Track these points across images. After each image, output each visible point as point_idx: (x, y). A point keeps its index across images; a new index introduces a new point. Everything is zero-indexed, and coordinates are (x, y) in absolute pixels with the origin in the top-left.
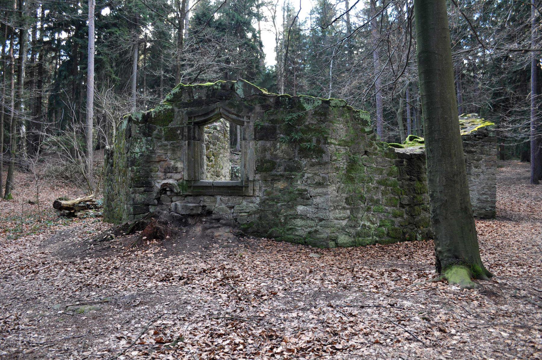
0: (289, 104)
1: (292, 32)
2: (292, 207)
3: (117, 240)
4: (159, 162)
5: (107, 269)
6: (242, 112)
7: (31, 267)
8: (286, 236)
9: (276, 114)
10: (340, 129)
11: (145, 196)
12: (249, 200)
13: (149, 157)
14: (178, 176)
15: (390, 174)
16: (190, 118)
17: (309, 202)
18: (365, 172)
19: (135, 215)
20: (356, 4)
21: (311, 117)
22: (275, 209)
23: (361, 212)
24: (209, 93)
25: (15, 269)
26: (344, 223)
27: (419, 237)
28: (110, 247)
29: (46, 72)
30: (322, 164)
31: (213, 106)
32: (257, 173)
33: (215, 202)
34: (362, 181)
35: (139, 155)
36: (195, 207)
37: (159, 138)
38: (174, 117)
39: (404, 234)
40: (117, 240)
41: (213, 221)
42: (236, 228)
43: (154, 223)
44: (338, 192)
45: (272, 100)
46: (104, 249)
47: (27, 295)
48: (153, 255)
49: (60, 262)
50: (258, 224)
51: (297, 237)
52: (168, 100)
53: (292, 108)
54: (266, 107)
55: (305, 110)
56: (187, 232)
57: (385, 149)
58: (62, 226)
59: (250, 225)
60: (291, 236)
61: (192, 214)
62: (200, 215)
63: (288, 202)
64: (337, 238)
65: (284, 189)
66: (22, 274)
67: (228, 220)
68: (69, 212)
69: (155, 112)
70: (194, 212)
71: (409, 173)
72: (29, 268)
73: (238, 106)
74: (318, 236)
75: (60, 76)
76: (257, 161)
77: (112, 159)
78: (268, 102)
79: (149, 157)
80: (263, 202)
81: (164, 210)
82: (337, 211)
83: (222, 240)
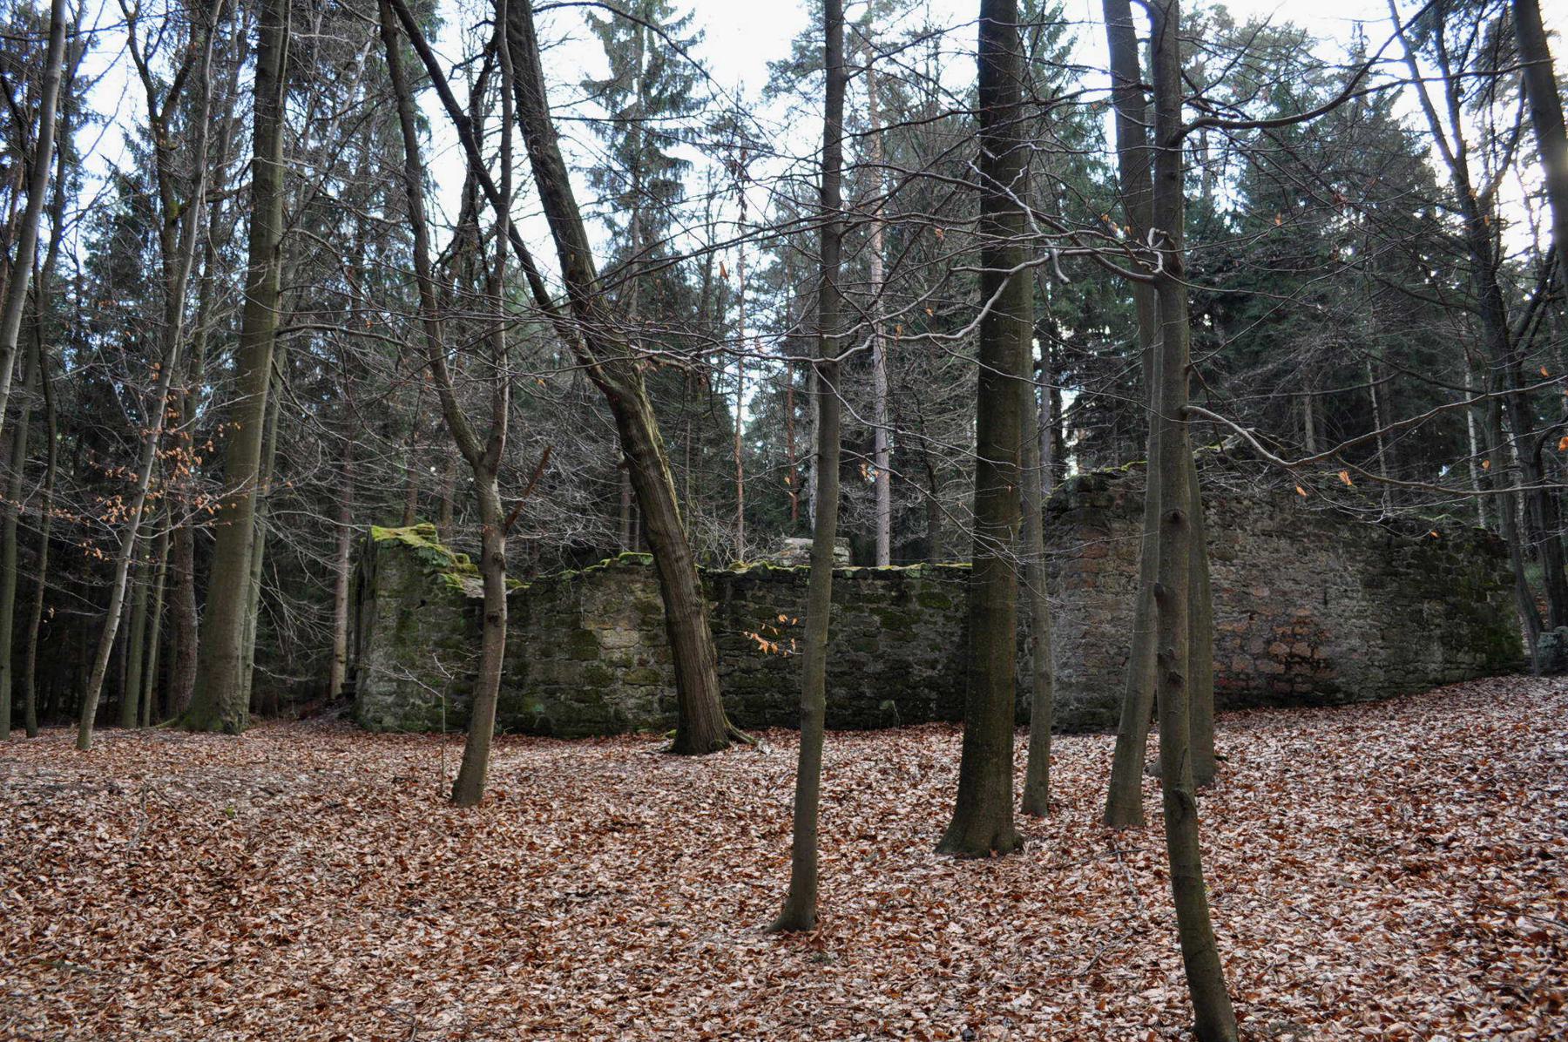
15: (454, 630)
20: (548, 7)
26: (390, 700)
34: (415, 642)
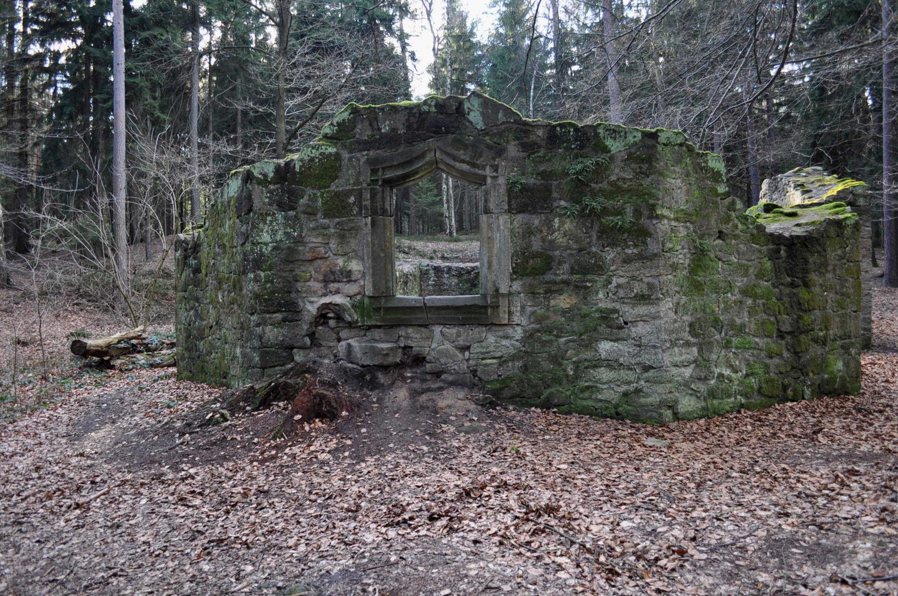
0: (576, 140)
1: (460, 38)
2: (589, 345)
3: (235, 422)
4: (311, 261)
5: (245, 495)
6: (480, 156)
7: (67, 492)
8: (579, 402)
9: (549, 160)
10: (676, 190)
11: (284, 331)
12: (501, 333)
13: (291, 251)
14: (352, 289)
15: (760, 275)
16: (374, 171)
17: (623, 334)
18: (719, 271)
19: (264, 369)
21: (622, 164)
22: (553, 350)
23: (715, 350)
24: (412, 119)
25: (32, 499)
26: (688, 372)
27: (808, 392)
28: (225, 438)
29: (33, 110)
30: (646, 258)
31: (421, 146)
32: (515, 279)
33: (430, 338)
34: (716, 290)
35: (269, 249)
36: (392, 349)
37: (311, 213)
38: (340, 170)
39: (785, 388)
40: (235, 422)
41: (428, 377)
42: (476, 389)
43: (311, 385)
44: (676, 312)
45: (540, 133)
46: (215, 444)
47: (81, 574)
48: (329, 456)
49: (129, 477)
50: (521, 381)
51: (600, 404)
52: (326, 137)
53: (582, 147)
54: (529, 148)
55: (609, 151)
56: (380, 401)
57: (751, 227)
58: (93, 389)
59: (505, 382)
60: (590, 403)
61: (385, 363)
62: (401, 365)
63: (581, 335)
64: (676, 402)
65: (570, 310)
66: (52, 513)
67: (458, 373)
68: (99, 360)
69: (301, 160)
70: (390, 360)
71: (791, 272)
72: (68, 495)
73: (473, 145)
74: (642, 400)
75: (60, 116)
76: (515, 254)
77: (195, 259)
78: (532, 138)
79: (291, 251)
80: (529, 337)
81: (325, 357)
82: (676, 349)
83: (456, 416)
